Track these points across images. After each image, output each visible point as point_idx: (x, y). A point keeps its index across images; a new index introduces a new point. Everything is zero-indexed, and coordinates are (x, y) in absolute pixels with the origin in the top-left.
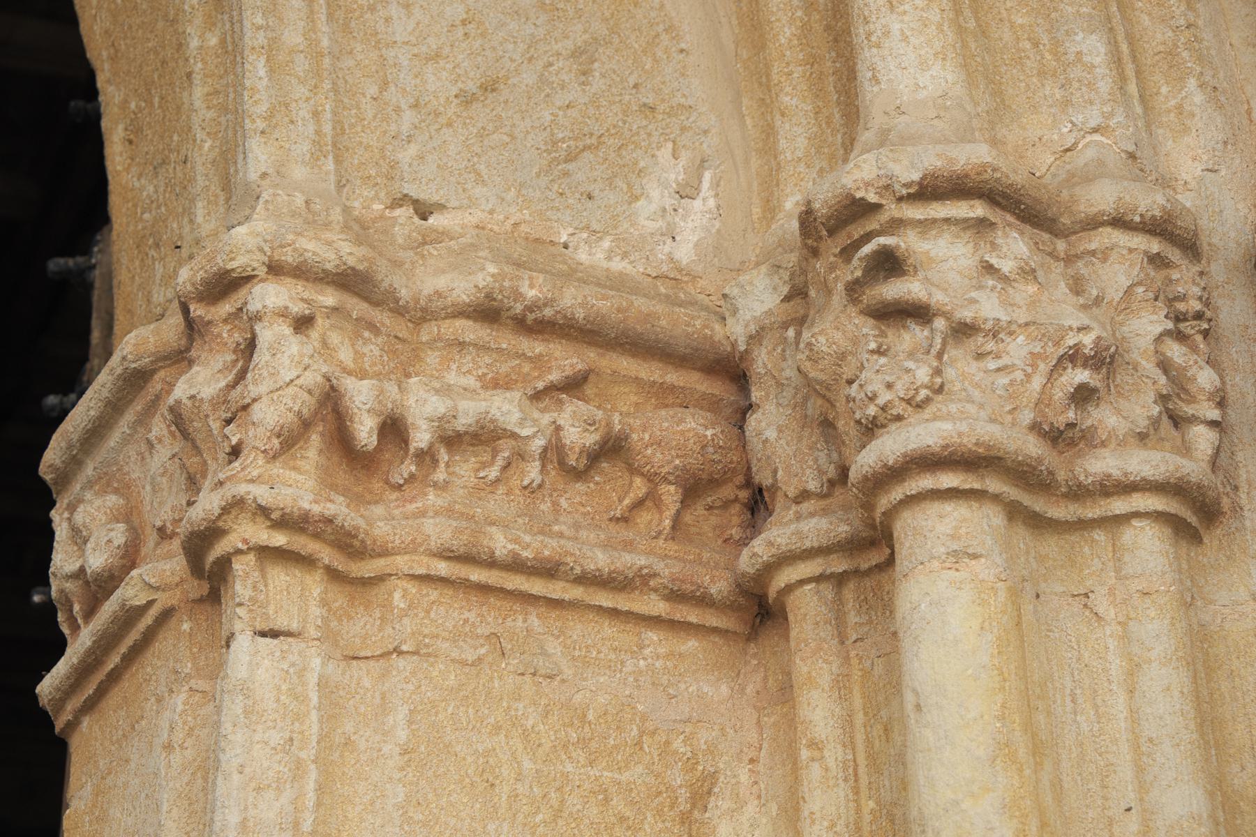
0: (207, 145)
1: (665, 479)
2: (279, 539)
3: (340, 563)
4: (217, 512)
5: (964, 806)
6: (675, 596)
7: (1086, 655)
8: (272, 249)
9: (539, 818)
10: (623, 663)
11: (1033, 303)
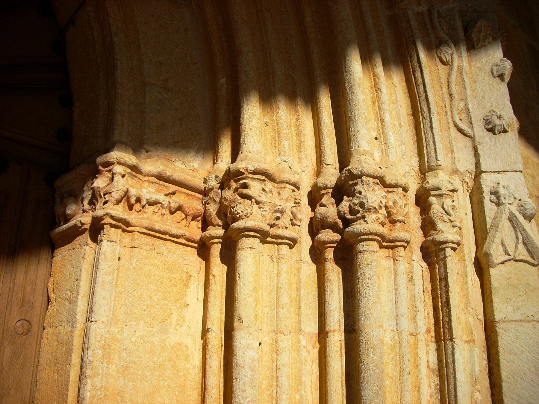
0: (102, 126)
1: (189, 215)
2: (114, 222)
3: (125, 228)
4: (103, 215)
5: (246, 299)
6: (188, 240)
7: (269, 268)
8: (119, 159)
9: (158, 284)
10: (176, 252)
11: (271, 198)
